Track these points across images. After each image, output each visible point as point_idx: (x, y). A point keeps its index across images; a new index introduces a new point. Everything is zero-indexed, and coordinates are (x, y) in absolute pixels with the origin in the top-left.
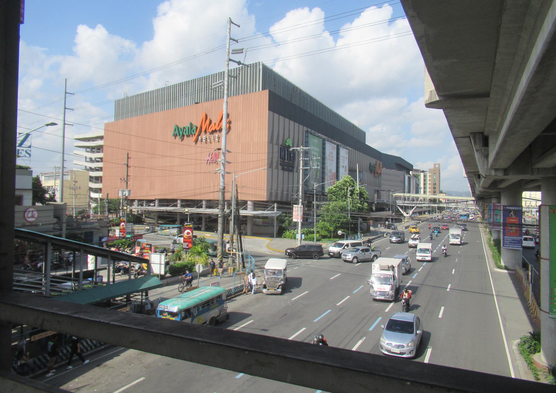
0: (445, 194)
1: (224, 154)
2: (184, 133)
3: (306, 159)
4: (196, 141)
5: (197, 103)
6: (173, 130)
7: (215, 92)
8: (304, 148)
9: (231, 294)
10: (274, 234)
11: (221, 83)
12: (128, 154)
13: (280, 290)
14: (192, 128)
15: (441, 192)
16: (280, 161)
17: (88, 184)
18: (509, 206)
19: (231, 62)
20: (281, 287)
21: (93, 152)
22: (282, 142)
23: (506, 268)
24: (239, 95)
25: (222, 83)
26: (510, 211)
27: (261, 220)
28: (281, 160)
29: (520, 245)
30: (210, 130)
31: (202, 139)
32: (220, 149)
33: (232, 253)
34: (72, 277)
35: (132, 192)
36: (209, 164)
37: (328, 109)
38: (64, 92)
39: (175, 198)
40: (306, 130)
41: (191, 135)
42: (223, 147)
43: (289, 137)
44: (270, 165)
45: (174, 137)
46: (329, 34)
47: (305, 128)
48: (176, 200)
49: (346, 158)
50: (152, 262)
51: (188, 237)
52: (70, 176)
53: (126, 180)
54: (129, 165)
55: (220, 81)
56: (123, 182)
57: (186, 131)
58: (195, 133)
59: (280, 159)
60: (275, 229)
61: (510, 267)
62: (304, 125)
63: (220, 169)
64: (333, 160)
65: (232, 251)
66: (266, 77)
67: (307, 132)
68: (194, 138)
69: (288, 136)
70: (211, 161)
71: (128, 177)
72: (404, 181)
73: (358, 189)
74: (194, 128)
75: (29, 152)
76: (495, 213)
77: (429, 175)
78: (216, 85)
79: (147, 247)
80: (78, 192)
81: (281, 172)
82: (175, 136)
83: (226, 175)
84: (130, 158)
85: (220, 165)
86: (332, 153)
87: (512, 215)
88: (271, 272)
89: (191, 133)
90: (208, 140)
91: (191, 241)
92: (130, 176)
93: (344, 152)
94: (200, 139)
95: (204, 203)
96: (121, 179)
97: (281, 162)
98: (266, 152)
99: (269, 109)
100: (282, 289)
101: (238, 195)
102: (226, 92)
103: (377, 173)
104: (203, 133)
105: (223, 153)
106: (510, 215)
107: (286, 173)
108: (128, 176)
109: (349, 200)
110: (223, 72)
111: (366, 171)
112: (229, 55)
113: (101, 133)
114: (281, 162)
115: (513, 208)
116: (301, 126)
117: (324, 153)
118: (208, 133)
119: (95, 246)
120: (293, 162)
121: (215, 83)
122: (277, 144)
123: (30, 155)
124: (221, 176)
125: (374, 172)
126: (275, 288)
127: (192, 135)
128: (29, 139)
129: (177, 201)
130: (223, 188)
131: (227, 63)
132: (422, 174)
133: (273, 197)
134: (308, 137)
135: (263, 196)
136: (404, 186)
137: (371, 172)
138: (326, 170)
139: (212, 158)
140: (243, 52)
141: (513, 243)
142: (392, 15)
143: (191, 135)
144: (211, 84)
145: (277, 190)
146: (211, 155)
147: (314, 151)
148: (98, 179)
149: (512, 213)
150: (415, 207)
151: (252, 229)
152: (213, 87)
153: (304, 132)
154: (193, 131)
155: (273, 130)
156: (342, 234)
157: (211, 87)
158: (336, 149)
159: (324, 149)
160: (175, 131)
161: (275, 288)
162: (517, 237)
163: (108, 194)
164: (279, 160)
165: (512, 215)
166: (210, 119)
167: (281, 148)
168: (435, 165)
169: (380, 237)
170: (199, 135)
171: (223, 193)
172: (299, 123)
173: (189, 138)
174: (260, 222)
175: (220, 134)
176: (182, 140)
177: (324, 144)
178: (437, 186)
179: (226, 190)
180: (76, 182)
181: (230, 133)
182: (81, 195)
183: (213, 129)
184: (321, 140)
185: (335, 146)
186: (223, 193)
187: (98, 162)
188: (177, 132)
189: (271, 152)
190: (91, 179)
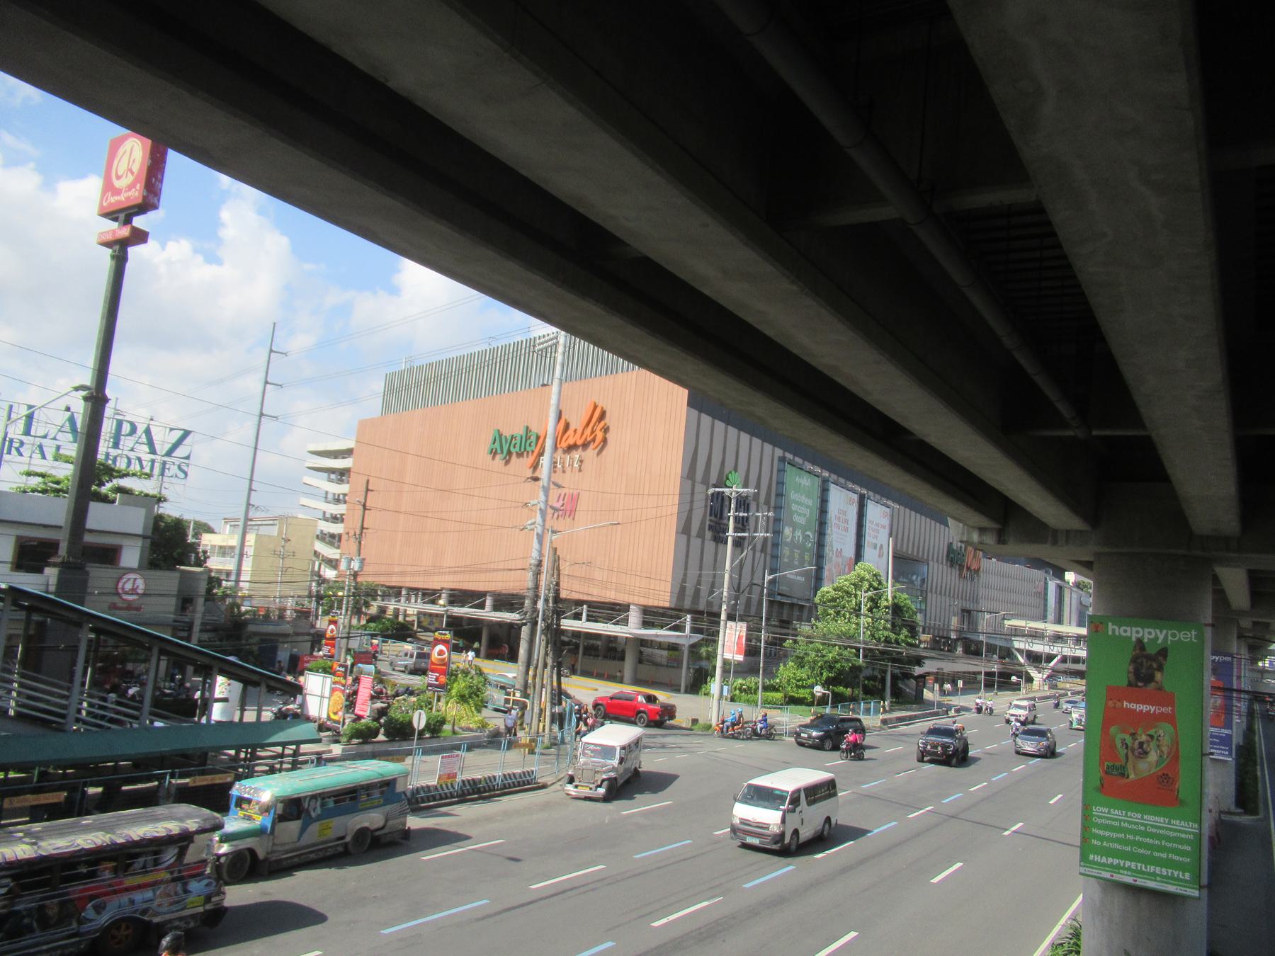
2: (512, 449)
5: (544, 385)
6: (491, 439)
7: (540, 357)
8: (739, 490)
9: (494, 786)
10: (680, 686)
12: (368, 482)
13: (602, 791)
16: (710, 520)
17: (313, 545)
20: (605, 783)
25: (555, 341)
27: (665, 653)
28: (713, 518)
29: (1226, 750)
30: (564, 445)
33: (514, 700)
40: (781, 455)
41: (525, 453)
43: (736, 469)
44: (685, 530)
47: (779, 452)
49: (884, 527)
51: (439, 659)
52: (277, 527)
54: (368, 504)
57: (515, 444)
58: (533, 448)
59: (711, 515)
60: (684, 675)
62: (775, 444)
64: (846, 529)
65: (514, 696)
67: (782, 459)
69: (733, 465)
71: (364, 531)
72: (1046, 594)
73: (890, 598)
75: (185, 468)
78: (542, 343)
80: (288, 562)
82: (494, 453)
84: (372, 491)
85: (536, 512)
86: (845, 513)
88: (592, 751)
90: (559, 466)
91: (444, 670)
99: (688, 405)
100: (609, 790)
101: (561, 579)
103: (968, 568)
108: (363, 528)
109: (864, 621)
111: (937, 561)
114: (712, 524)
116: (768, 448)
117: (823, 510)
118: (560, 451)
119: (231, 658)
123: (186, 474)
124: (535, 536)
125: (961, 567)
126: (591, 786)
127: (528, 452)
128: (188, 440)
129: (628, 610)
130: (536, 563)
133: (686, 598)
134: (784, 471)
135: (663, 598)
136: (1046, 605)
137: (952, 566)
138: (827, 550)
143: (525, 453)
145: (699, 583)
146: (562, 497)
147: (799, 503)
150: (1059, 657)
151: (635, 671)
152: (538, 348)
154: (530, 445)
156: (824, 694)
157: (534, 346)
159: (824, 501)
160: (494, 443)
161: (591, 786)
162: (1221, 728)
164: (708, 518)
166: (566, 420)
169: (937, 714)
172: (764, 440)
174: (662, 656)
175: (583, 454)
176: (507, 462)
177: (825, 491)
180: (288, 540)
181: (604, 452)
183: (571, 441)
184: (817, 482)
185: (856, 497)
188: (497, 445)
190: (322, 537)
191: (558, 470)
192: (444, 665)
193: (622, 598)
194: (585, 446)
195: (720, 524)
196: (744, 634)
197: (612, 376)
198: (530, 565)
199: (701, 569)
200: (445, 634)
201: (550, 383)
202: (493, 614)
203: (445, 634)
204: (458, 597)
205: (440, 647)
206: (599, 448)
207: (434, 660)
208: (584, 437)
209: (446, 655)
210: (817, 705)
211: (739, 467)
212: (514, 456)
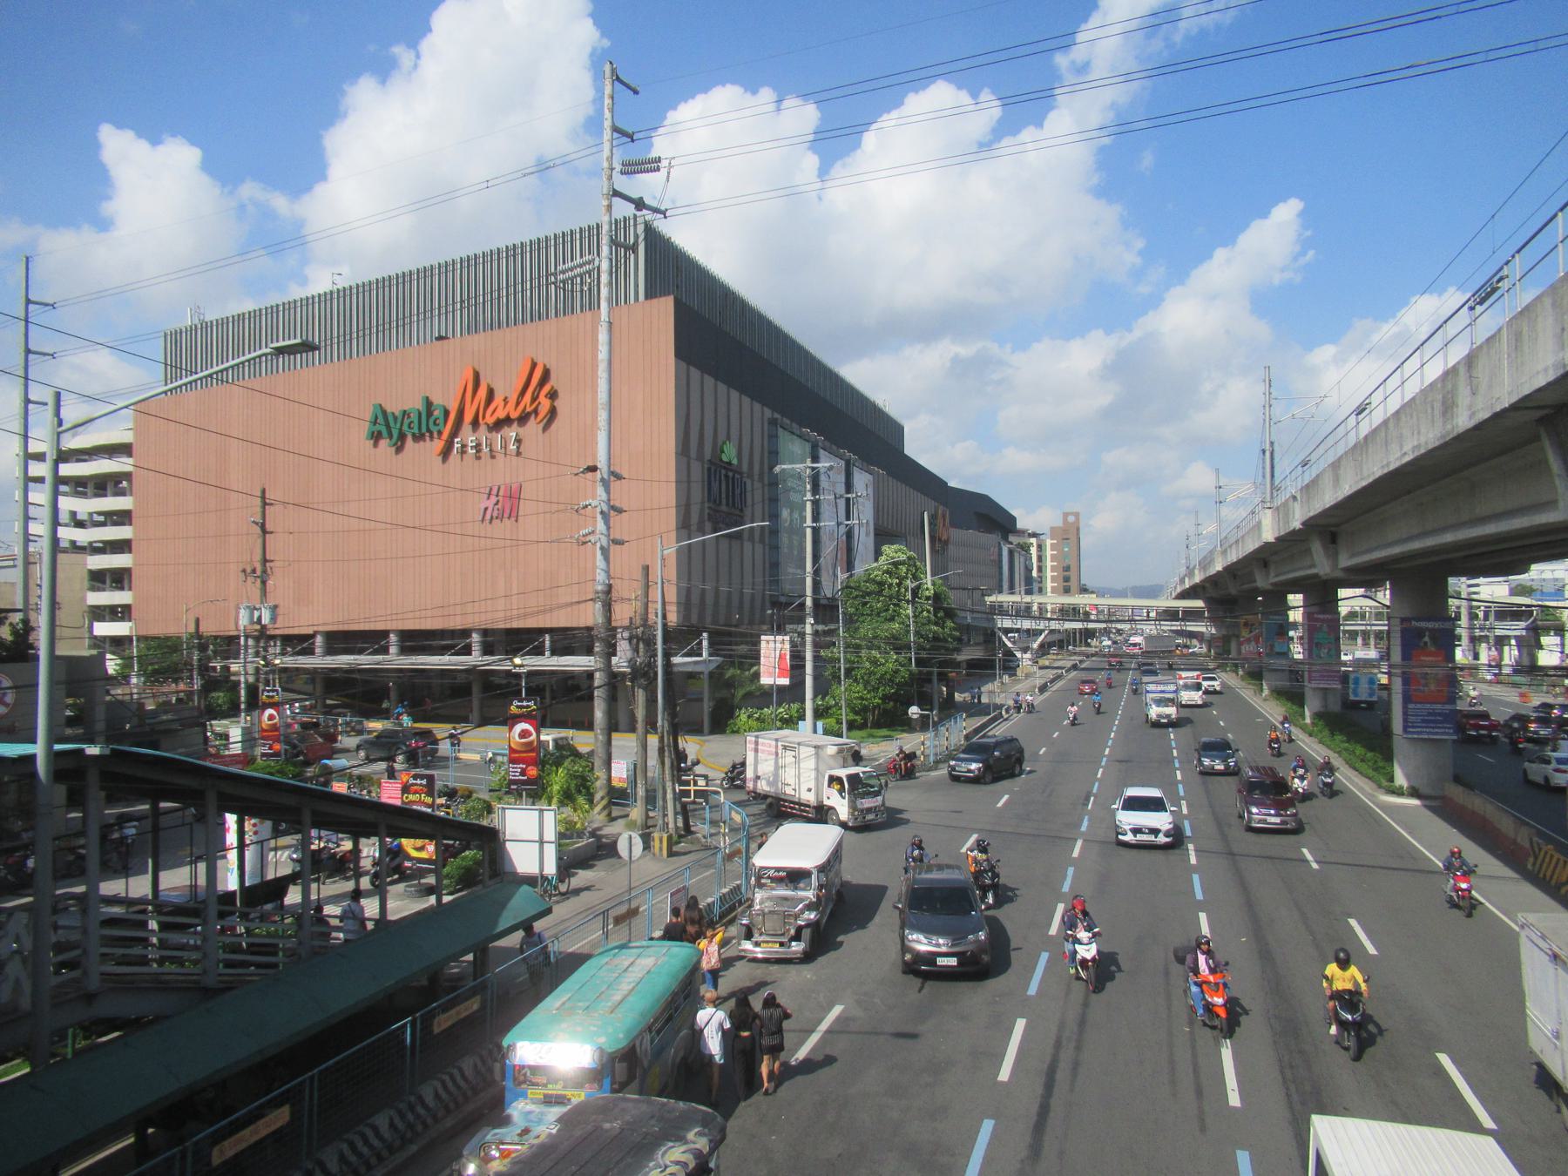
0: (1094, 596)
1: (606, 483)
4: (446, 453)
5: (440, 338)
10: (702, 726)
11: (589, 263)
14: (429, 413)
15: (1084, 590)
16: (709, 508)
18: (1418, 620)
19: (616, 200)
21: (84, 495)
22: (713, 450)
23: (1414, 793)
24: (573, 313)
26: (1420, 633)
28: (711, 505)
29: (1449, 728)
30: (491, 420)
31: (464, 446)
32: (593, 469)
33: (695, 791)
34: (238, 904)
35: (280, 611)
36: (491, 522)
38: (23, 300)
39: (380, 626)
42: (602, 462)
43: (729, 438)
45: (372, 442)
46: (998, 103)
47: (768, 413)
48: (384, 634)
50: (507, 838)
53: (262, 574)
55: (587, 258)
56: (250, 579)
59: (709, 500)
61: (1425, 790)
63: (593, 532)
65: (695, 784)
66: (656, 264)
67: (773, 422)
68: (438, 445)
70: (495, 514)
71: (268, 564)
72: (1000, 561)
74: (437, 413)
76: (1316, 641)
77: (1052, 544)
79: (416, 784)
82: (376, 437)
83: (613, 548)
89: (428, 430)
90: (485, 450)
92: (272, 561)
93: (862, 480)
95: (476, 638)
96: (244, 571)
97: (711, 512)
98: (673, 478)
99: (681, 353)
102: (604, 291)
103: (940, 540)
104: (466, 427)
105: (602, 480)
106: (1422, 644)
108: (265, 561)
110: (598, 225)
112: (610, 177)
113: (127, 437)
115: (1430, 625)
116: (757, 406)
118: (483, 428)
120: (741, 510)
121: (569, 265)
122: (700, 457)
124: (599, 553)
129: (470, 636)
131: (605, 203)
132: (1033, 540)
134: (776, 436)
136: (1001, 574)
139: (498, 501)
140: (658, 169)
142: (817, 127)
144: (556, 269)
148: (119, 579)
149: (1426, 639)
152: (561, 277)
155: (688, 415)
156: (921, 715)
158: (843, 473)
162: (1444, 703)
163: (197, 621)
164: (706, 505)
165: (1426, 643)
167: (709, 469)
168: (1066, 515)
170: (455, 432)
171: (608, 607)
173: (422, 443)
175: (521, 430)
178: (1073, 574)
179: (614, 594)
181: (554, 426)
182: (440, 614)
183: (501, 414)
185: (843, 463)
186: (608, 607)
187: (103, 524)
189: (684, 481)
191: (482, 454)
192: (532, 750)
194: (523, 419)
195: (718, 511)
196: (788, 653)
197: (534, 324)
199: (753, 577)
200: (528, 707)
201: (450, 335)
202: (329, 659)
204: (340, 641)
205: (270, 711)
206: (545, 421)
207: (264, 726)
208: (521, 408)
210: (871, 728)
212: (409, 439)
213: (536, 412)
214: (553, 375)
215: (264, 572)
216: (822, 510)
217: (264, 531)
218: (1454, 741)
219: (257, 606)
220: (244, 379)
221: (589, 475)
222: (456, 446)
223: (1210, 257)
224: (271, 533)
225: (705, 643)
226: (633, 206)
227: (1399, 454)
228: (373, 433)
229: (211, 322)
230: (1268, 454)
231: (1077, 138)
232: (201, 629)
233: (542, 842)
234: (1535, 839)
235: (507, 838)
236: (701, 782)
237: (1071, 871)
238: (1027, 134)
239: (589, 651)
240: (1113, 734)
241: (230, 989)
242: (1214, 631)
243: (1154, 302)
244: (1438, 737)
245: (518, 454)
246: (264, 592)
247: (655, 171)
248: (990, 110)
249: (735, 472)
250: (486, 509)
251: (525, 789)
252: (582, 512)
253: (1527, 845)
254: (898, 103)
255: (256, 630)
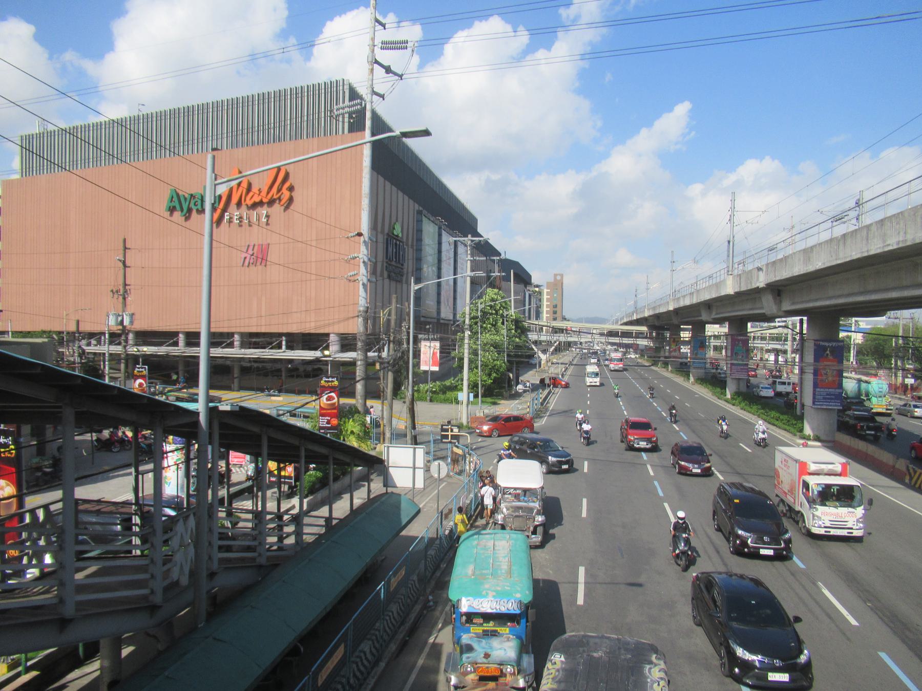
2: (192, 205)
3: (477, 258)
12: (125, 241)
15: (564, 319)
19: (376, 66)
24: (301, 138)
26: (824, 349)
30: (249, 202)
33: (451, 435)
35: (136, 317)
37: (433, 175)
43: (397, 221)
46: (527, 33)
47: (417, 206)
51: (329, 404)
53: (123, 293)
56: (116, 296)
59: (387, 258)
61: (823, 438)
65: (452, 431)
70: (251, 262)
71: (127, 287)
73: (513, 314)
76: (735, 351)
77: (547, 292)
81: (387, 281)
82: (172, 210)
87: (827, 355)
92: (129, 285)
94: (226, 217)
96: (112, 291)
104: (233, 206)
107: (393, 284)
108: (125, 285)
118: (244, 207)
120: (402, 265)
122: (382, 232)
124: (361, 287)
129: (233, 336)
134: (422, 221)
141: (828, 399)
146: (251, 248)
149: (828, 352)
153: (415, 213)
162: (836, 389)
163: (78, 322)
164: (385, 260)
165: (827, 355)
167: (387, 239)
168: (555, 275)
170: (225, 210)
173: (202, 215)
175: (270, 210)
176: (187, 218)
177: (440, 235)
178: (558, 309)
183: (257, 199)
193: (172, 328)
194: (271, 203)
196: (438, 351)
197: (249, 147)
198: (360, 312)
200: (332, 381)
203: (332, 381)
205: (140, 381)
209: (336, 400)
211: (399, 220)
212: (194, 213)
213: (279, 199)
214: (291, 176)
215: (126, 291)
216: (442, 267)
217: (125, 266)
218: (838, 410)
219: (120, 314)
220: (77, 169)
221: (357, 238)
222: (226, 217)
223: (638, 132)
224: (129, 267)
225: (284, 343)
226: (384, 70)
227: (881, 245)
228: (170, 207)
229: (33, 135)
230: (731, 243)
231: (568, 58)
232: (80, 329)
233: (414, 468)
234: (911, 466)
235: (390, 465)
236: (456, 430)
237: (656, 483)
238: (541, 54)
239: (355, 350)
240: (621, 403)
241: (276, 565)
242: (652, 345)
243: (606, 156)
244: (830, 407)
245: (267, 224)
246: (125, 304)
247: (404, 49)
248: (523, 38)
249: (400, 241)
250: (245, 258)
251: (329, 433)
252: (352, 262)
253: (904, 469)
254: (469, 26)
255: (119, 330)
